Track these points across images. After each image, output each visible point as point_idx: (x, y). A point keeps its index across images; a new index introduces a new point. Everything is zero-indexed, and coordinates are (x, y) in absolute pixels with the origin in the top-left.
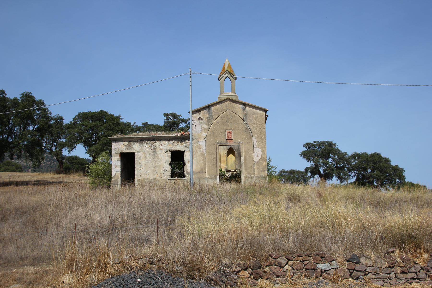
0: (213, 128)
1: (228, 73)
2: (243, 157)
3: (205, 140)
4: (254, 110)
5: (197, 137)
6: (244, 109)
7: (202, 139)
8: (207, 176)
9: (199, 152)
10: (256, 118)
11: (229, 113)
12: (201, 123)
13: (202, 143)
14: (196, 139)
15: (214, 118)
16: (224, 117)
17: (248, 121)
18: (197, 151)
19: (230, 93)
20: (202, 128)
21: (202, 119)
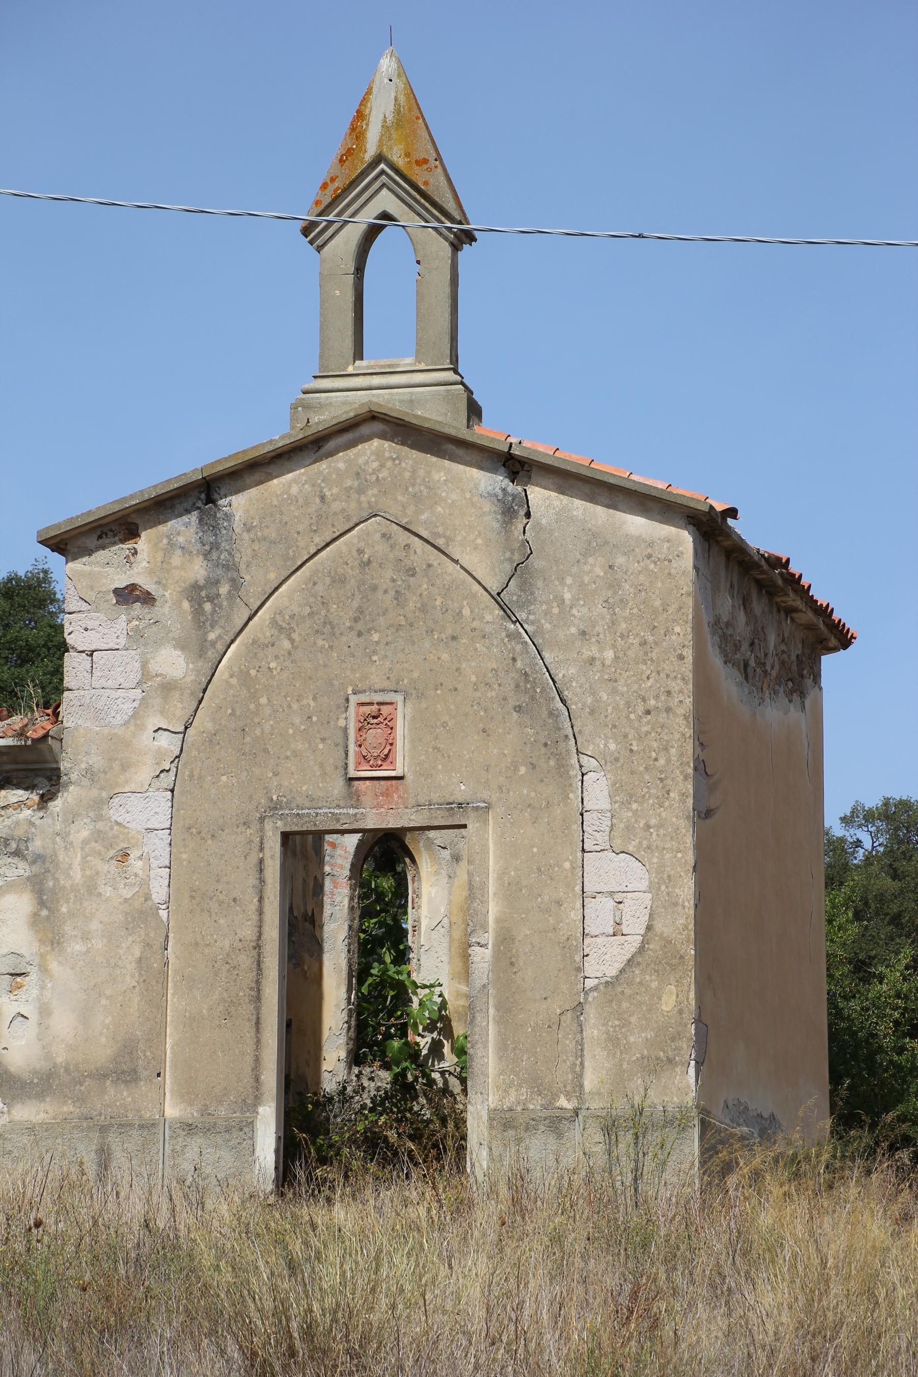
0: (244, 678)
1: (391, 188)
2: (489, 938)
3: (167, 780)
4: (599, 514)
5: (96, 760)
6: (513, 510)
7: (144, 774)
8: (172, 1111)
9: (116, 893)
10: (614, 585)
11: (381, 548)
12: (136, 637)
13: (144, 812)
14: (90, 773)
15: (252, 594)
16: (339, 580)
17: (539, 616)
18: (91, 888)
19: (407, 362)
20: (146, 675)
21: (148, 599)
